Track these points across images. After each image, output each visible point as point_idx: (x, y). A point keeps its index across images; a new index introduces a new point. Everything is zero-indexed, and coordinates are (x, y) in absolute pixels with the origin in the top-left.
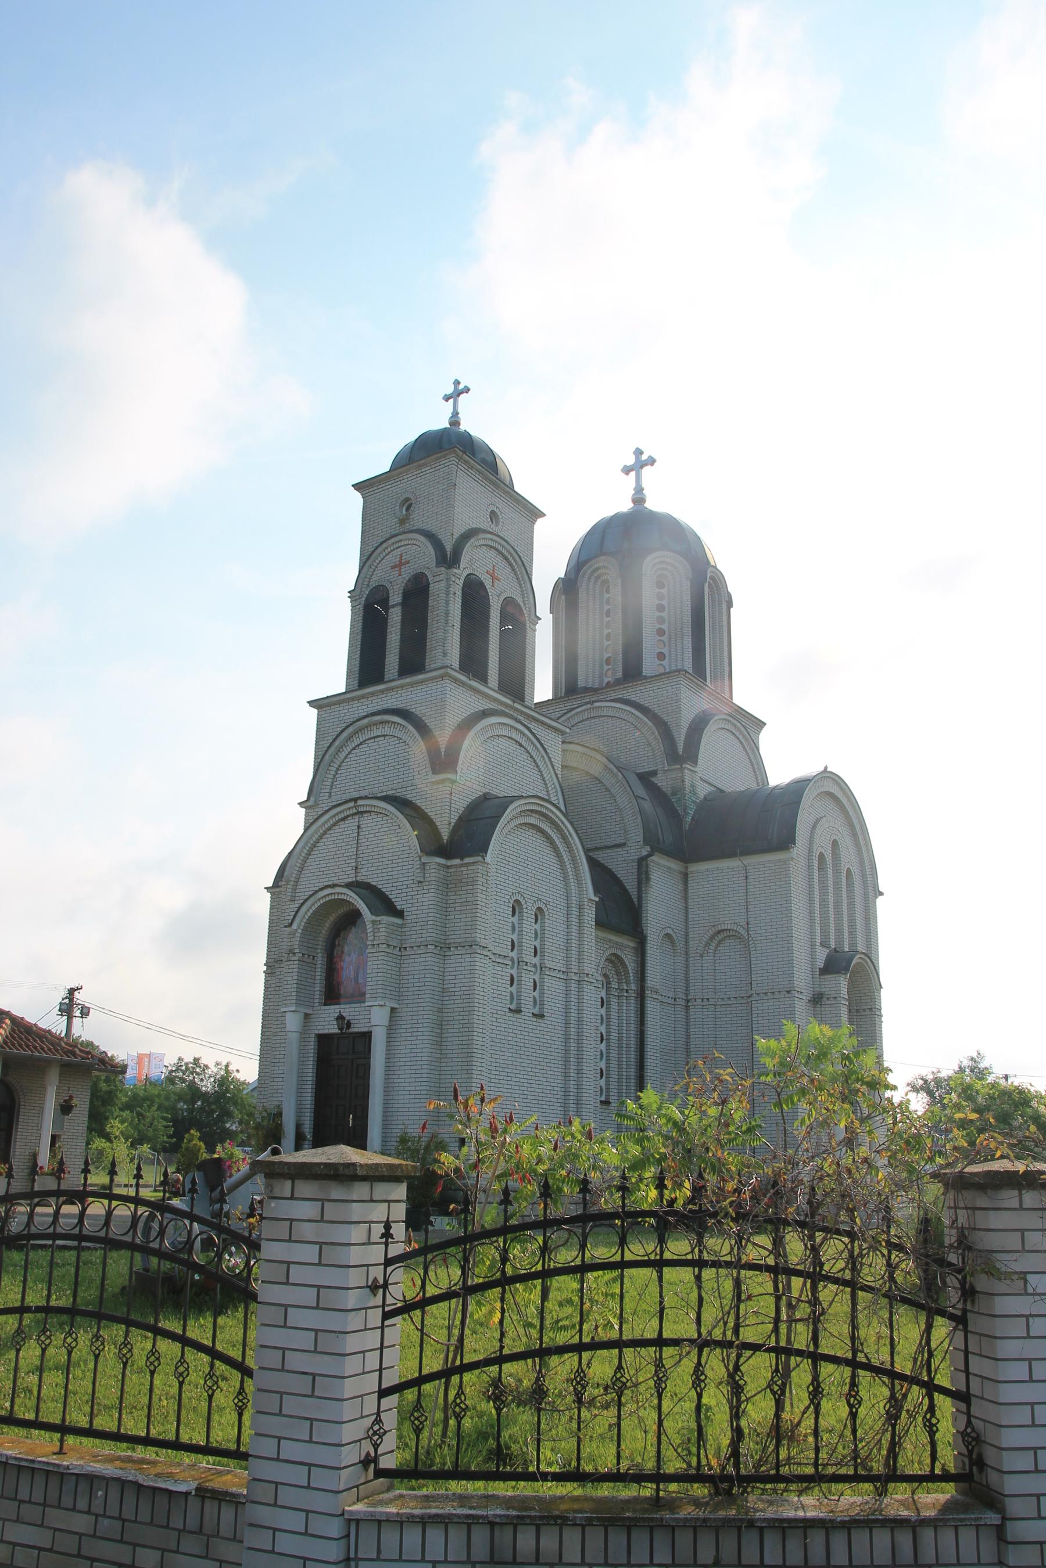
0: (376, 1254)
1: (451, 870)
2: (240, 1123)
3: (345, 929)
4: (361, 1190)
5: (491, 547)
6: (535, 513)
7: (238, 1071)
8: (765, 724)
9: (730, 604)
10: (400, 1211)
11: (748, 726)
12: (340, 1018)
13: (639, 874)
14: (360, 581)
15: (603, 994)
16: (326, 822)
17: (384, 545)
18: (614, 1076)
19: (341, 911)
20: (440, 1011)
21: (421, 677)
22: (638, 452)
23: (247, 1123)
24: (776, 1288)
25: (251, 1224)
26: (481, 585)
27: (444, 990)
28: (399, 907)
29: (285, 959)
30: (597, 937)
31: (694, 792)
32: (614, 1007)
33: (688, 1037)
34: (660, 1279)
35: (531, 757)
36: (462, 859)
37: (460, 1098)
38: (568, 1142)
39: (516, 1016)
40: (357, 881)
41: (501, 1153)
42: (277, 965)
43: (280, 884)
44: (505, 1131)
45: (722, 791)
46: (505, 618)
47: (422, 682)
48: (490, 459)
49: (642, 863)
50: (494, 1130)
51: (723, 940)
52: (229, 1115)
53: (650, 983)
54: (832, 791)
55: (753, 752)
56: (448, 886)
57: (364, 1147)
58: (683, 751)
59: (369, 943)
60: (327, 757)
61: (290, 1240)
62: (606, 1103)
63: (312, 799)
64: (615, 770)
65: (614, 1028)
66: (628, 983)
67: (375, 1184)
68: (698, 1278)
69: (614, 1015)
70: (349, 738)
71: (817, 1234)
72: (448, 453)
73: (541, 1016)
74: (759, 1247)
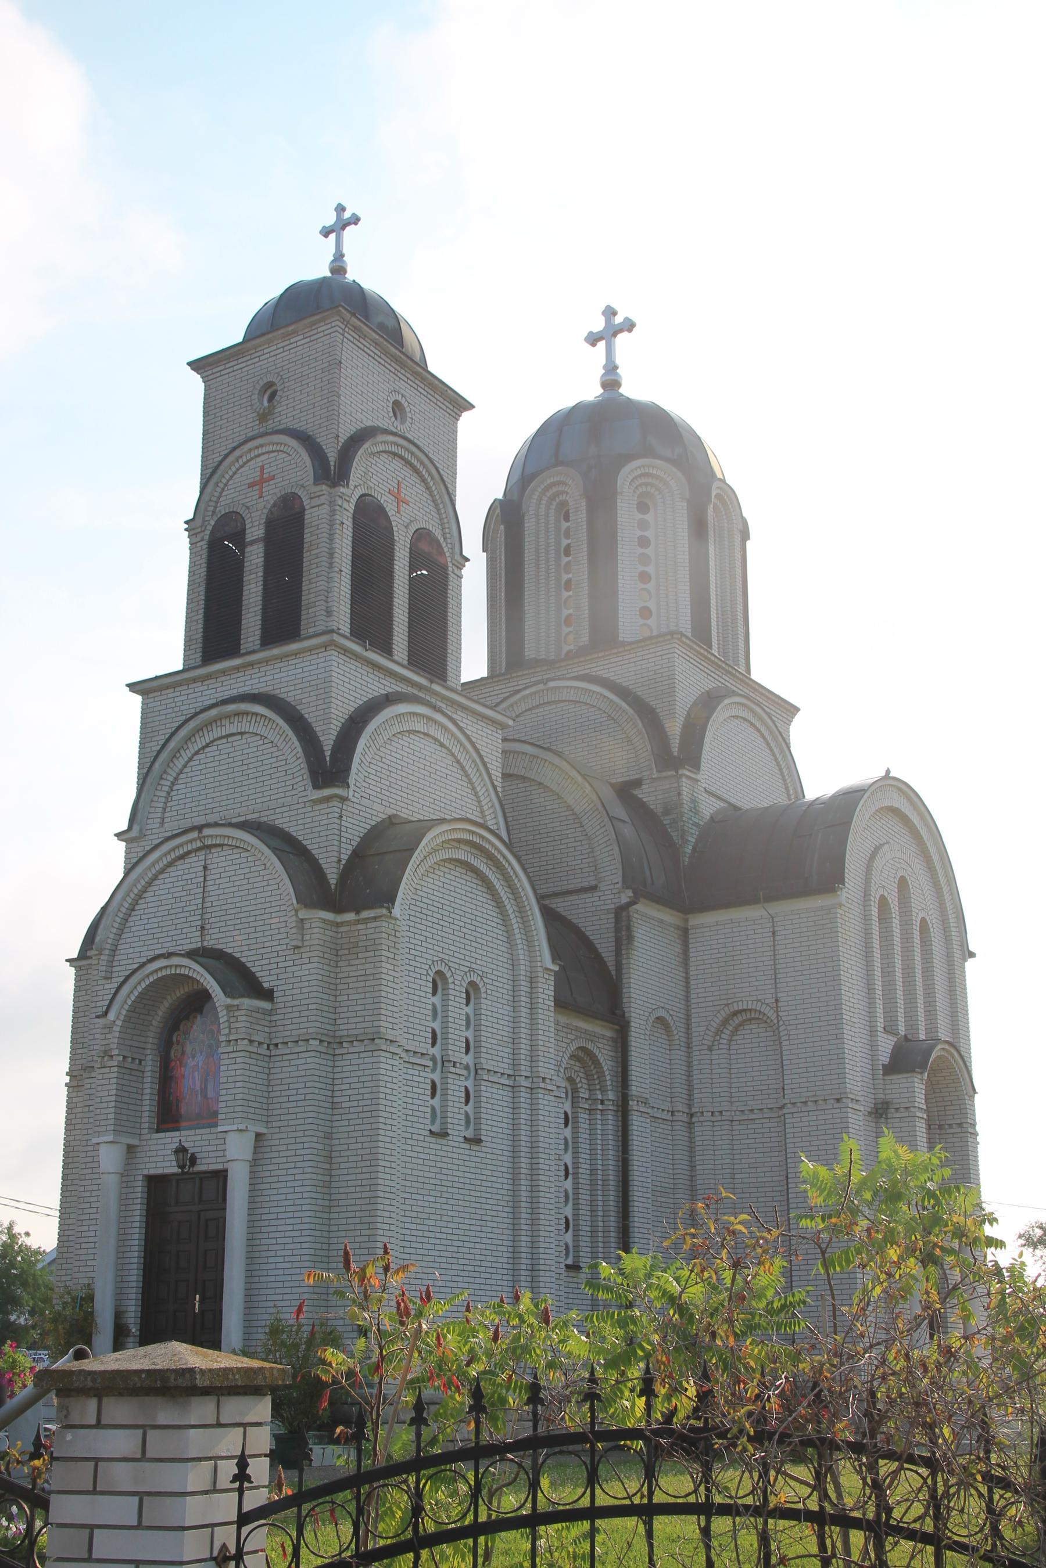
0: (226, 1507)
1: (342, 929)
2: (32, 1313)
3: (187, 1018)
4: (202, 1410)
5: (395, 454)
6: (459, 405)
7: (27, 1234)
8: (798, 710)
9: (745, 535)
10: (262, 1440)
11: (774, 714)
12: (181, 1150)
13: (617, 929)
14: (202, 506)
15: (567, 1107)
16: (157, 861)
17: (237, 453)
18: (585, 1228)
19: (180, 993)
20: (329, 1136)
21: (294, 646)
22: (610, 313)
23: (42, 1313)
24: (822, 1546)
25: (35, 1468)
26: (381, 510)
27: (334, 1106)
28: (266, 985)
29: (97, 1065)
30: (557, 1023)
31: (695, 810)
32: (584, 1126)
33: (692, 1167)
34: (649, 1534)
35: (458, 762)
36: (358, 913)
37: (353, 1265)
38: (514, 1327)
39: (440, 1141)
40: (204, 949)
41: (414, 1347)
42: (86, 1075)
43: (89, 954)
44: (420, 1314)
45: (737, 808)
46: (416, 559)
47: (296, 654)
48: (391, 323)
49: (621, 915)
50: (403, 1313)
51: (741, 1024)
52: (15, 1302)
53: (635, 1090)
54: (898, 807)
55: (782, 751)
56: (339, 953)
57: (216, 1345)
58: (682, 754)
59: (222, 1038)
60: (157, 765)
61: (94, 1492)
62: (574, 1268)
63: (136, 828)
64: (580, 779)
65: (584, 1157)
66: (603, 1090)
67: (222, 1398)
68: (706, 1532)
69: (584, 1136)
70: (189, 739)
71: (881, 1462)
72: (328, 318)
73: (477, 1141)
74: (793, 1486)
